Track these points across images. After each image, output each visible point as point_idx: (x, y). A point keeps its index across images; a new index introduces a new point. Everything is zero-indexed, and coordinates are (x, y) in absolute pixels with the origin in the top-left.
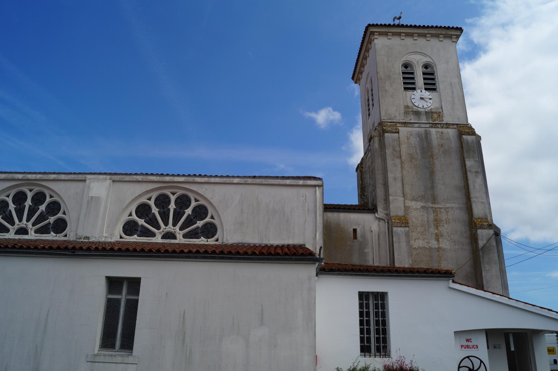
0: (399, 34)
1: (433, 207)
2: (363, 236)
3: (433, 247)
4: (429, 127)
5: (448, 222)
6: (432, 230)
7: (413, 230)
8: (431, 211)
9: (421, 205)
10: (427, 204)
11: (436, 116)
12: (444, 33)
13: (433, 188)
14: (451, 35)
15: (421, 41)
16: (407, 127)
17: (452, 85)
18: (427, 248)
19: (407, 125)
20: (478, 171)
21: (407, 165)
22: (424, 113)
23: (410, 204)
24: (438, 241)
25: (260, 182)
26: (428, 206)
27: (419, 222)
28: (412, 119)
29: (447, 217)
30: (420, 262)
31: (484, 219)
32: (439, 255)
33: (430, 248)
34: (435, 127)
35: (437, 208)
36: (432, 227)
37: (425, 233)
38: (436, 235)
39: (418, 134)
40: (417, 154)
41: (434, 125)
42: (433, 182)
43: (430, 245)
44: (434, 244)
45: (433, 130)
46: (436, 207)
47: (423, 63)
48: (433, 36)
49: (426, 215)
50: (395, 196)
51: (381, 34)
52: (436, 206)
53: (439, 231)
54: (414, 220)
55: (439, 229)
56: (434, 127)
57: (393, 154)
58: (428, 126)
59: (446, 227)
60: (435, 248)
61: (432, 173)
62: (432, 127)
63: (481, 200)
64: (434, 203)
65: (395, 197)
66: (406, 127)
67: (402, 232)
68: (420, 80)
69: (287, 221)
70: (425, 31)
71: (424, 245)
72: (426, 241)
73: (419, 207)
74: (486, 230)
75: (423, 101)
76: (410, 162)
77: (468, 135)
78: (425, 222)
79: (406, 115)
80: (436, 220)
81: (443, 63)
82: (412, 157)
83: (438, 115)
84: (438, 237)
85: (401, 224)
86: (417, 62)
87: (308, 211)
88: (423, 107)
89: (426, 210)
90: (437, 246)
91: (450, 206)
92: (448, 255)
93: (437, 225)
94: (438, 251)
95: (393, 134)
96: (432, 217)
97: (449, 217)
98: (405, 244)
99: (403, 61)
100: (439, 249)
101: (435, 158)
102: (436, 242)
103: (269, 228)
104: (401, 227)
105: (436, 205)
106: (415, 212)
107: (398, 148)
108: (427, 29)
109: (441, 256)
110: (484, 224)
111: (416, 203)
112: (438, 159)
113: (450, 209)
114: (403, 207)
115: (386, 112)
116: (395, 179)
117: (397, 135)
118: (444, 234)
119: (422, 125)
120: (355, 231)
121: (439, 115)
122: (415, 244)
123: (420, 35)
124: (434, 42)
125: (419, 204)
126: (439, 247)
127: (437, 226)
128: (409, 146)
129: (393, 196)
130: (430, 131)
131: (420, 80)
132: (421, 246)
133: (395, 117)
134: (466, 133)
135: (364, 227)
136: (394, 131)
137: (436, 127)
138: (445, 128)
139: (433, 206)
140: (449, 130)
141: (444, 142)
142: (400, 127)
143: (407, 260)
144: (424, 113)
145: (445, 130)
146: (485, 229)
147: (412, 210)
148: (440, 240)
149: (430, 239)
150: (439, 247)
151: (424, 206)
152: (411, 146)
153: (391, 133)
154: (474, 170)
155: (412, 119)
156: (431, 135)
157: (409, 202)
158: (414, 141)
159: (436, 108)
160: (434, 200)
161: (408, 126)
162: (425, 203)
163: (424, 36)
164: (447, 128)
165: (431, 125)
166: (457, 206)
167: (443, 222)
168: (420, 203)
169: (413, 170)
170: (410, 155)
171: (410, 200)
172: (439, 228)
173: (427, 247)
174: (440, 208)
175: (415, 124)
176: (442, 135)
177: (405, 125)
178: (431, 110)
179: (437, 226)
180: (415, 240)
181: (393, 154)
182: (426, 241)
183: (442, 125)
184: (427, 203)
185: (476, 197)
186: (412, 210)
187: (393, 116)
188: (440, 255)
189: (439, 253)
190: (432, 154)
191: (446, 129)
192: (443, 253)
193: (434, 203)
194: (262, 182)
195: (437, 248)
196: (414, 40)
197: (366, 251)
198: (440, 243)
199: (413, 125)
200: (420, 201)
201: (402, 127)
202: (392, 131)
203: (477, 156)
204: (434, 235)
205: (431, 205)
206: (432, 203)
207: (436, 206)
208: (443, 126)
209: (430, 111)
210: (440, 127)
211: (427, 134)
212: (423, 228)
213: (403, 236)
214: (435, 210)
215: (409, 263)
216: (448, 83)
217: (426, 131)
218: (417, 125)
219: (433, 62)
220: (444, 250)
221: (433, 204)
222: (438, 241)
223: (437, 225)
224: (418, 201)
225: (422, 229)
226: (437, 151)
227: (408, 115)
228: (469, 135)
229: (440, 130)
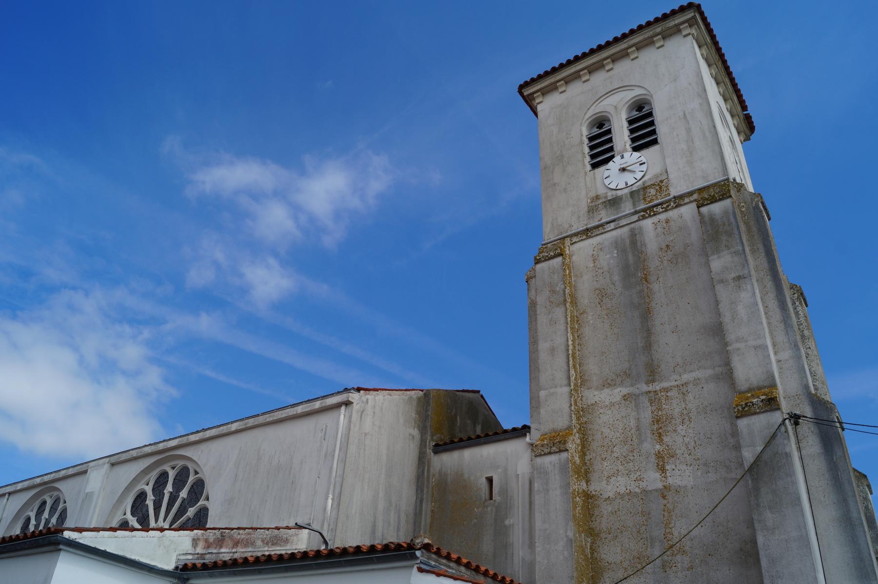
0: (576, 76)
1: (650, 392)
2: (504, 491)
3: (650, 489)
4: (637, 221)
5: (687, 418)
6: (650, 446)
7: (604, 457)
8: (645, 401)
9: (621, 394)
10: (637, 386)
11: (652, 191)
12: (658, 30)
13: (648, 346)
14: (676, 25)
15: (623, 67)
16: (593, 237)
17: (688, 116)
18: (636, 495)
19: (592, 234)
20: (741, 274)
21: (591, 314)
22: (629, 196)
23: (597, 399)
24: (663, 470)
25: (263, 420)
26: (638, 392)
27: (618, 435)
28: (604, 216)
29: (684, 406)
30: (619, 531)
31: (765, 387)
32: (665, 506)
33: (645, 492)
34: (650, 216)
35: (660, 390)
36: (649, 440)
37: (632, 458)
38: (659, 456)
39: (616, 242)
40: (614, 284)
41: (649, 212)
42: (648, 333)
43: (643, 485)
44: (653, 479)
45: (648, 223)
46: (658, 388)
47: (626, 103)
48: (639, 47)
49: (634, 413)
50: (551, 388)
51: (545, 92)
52: (657, 386)
53: (664, 446)
54: (606, 431)
55: (666, 439)
56: (647, 216)
57: (550, 301)
58: (635, 218)
59: (683, 433)
60: (656, 490)
61: (646, 314)
62: (644, 218)
63: (752, 343)
64: (653, 381)
65: (552, 390)
66: (591, 237)
67: (554, 466)
68: (621, 136)
69: (293, 482)
70: (622, 46)
71: (628, 488)
72: (633, 476)
73: (618, 398)
74: (762, 417)
75: (626, 174)
76: (599, 306)
77: (712, 203)
78: (632, 432)
79: (591, 215)
80: (657, 420)
81: (666, 85)
82: (602, 294)
83: (658, 188)
84: (661, 463)
85: (551, 447)
86: (616, 107)
87: (326, 456)
88: (627, 184)
89: (633, 402)
90: (660, 485)
91: (691, 379)
92: (689, 503)
93: (661, 431)
94: (664, 497)
95: (551, 262)
96: (647, 415)
97: (690, 406)
98: (558, 492)
99: (591, 117)
100: (664, 492)
101: (652, 278)
102: (657, 475)
103: (266, 501)
104: (550, 453)
105: (656, 384)
106: (609, 412)
107: (561, 285)
108: (624, 40)
109: (671, 507)
110: (752, 403)
111: (611, 393)
112: (661, 279)
113: (691, 385)
114: (568, 408)
115: (553, 225)
116: (553, 350)
117: (560, 259)
118: (678, 451)
119: (623, 222)
120: (490, 480)
121: (661, 188)
122: (610, 488)
123: (615, 59)
124: (649, 56)
125: (618, 392)
126: (665, 487)
127: (660, 435)
128: (597, 273)
129: (547, 389)
130: (640, 228)
131: (621, 136)
132: (622, 492)
133: (571, 226)
134: (707, 199)
135: (506, 470)
136: (551, 255)
137: (652, 214)
138: (673, 208)
139: (651, 388)
140: (683, 210)
141: (671, 238)
142: (579, 241)
143: (561, 532)
144: (627, 197)
145: (673, 214)
146: (755, 413)
147: (601, 411)
148: (667, 467)
149: (643, 470)
150: (665, 487)
151: (628, 394)
152: (600, 271)
153: (546, 260)
154: (733, 275)
155: (604, 216)
156: (642, 235)
157: (596, 393)
158: (608, 260)
159: (655, 175)
160: (652, 373)
161: (593, 235)
162: (632, 385)
163: (624, 55)
164: (677, 207)
165: (642, 213)
166: (710, 372)
167: (673, 422)
168: (619, 389)
169: (605, 321)
170: (598, 292)
171: (597, 389)
172: (664, 438)
173: (637, 490)
174: (667, 390)
175: (608, 225)
176: (668, 224)
177: (587, 236)
178: (644, 185)
179: (660, 435)
180: (609, 477)
181: (550, 301)
182: (633, 476)
183: (665, 206)
184: (635, 384)
185: (739, 340)
186: (601, 411)
187: (566, 226)
188: (668, 505)
189: (666, 502)
190: (646, 274)
191: (676, 211)
192: (675, 498)
193: (651, 380)
194: (266, 419)
195: (660, 490)
196: (608, 71)
197: (507, 522)
198: (668, 474)
199: (604, 229)
200: (619, 384)
201: (582, 240)
202: (547, 256)
203: (738, 241)
204: (653, 459)
205: (644, 388)
206: (647, 383)
207: (657, 386)
208: (668, 206)
209: (643, 186)
210: (661, 210)
211: (636, 235)
212: (627, 447)
213: (555, 474)
214: (654, 398)
215: (567, 536)
216: (679, 116)
217: (632, 231)
218: (612, 225)
219: (650, 94)
220: (678, 490)
221: (650, 385)
222: (663, 470)
223: (661, 431)
224: (615, 387)
225: (624, 449)
226: (658, 263)
227: (595, 214)
228: (716, 201)
229: (663, 217)
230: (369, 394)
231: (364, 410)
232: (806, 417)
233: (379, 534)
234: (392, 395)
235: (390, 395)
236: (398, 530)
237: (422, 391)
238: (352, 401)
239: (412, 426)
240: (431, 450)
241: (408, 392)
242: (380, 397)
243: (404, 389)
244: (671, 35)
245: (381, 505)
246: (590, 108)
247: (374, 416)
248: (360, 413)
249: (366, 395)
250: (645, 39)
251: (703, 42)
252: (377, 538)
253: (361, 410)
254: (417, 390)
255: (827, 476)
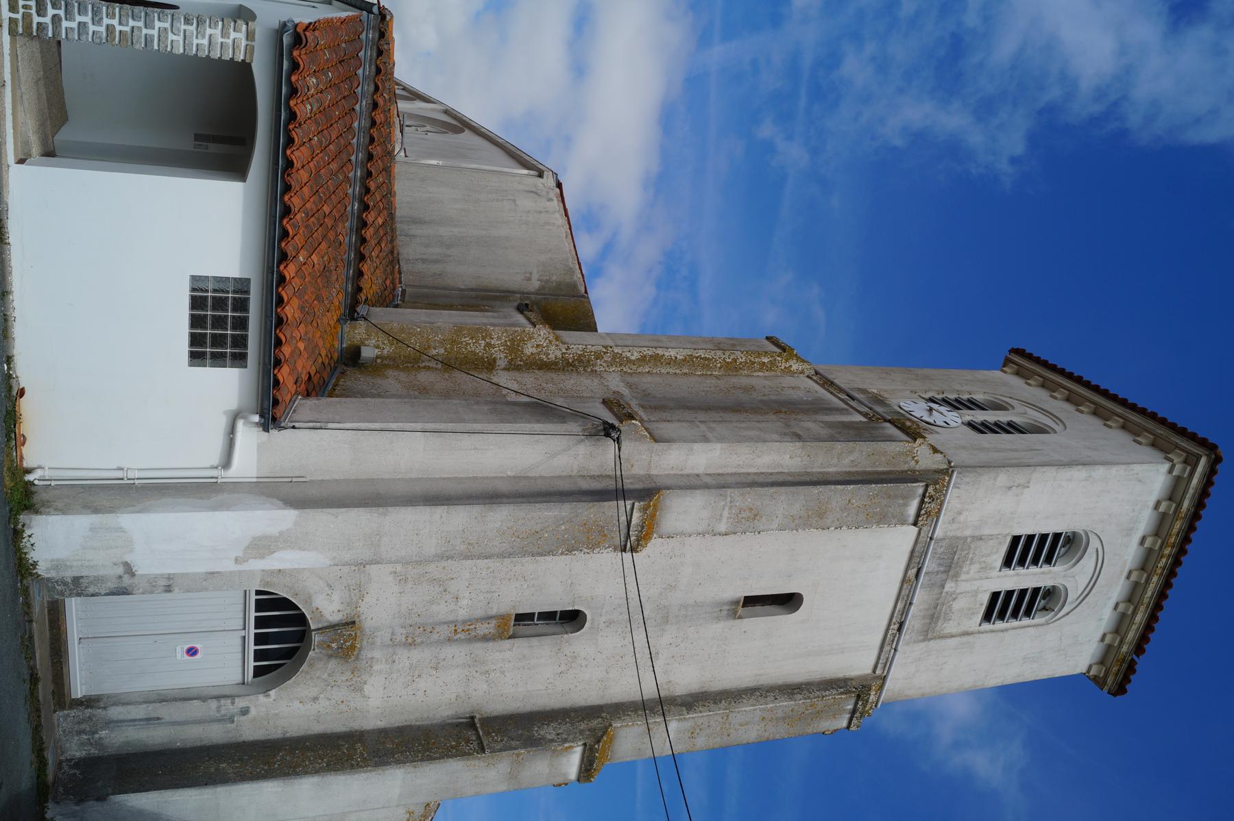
218: (844, 397)
230: (558, 201)
231: (539, 195)
232: (619, 450)
233: (415, 230)
234: (568, 239)
235: (566, 237)
236: (424, 261)
237: (586, 292)
238: (545, 176)
239: (541, 276)
240: (519, 301)
241: (577, 266)
242: (561, 220)
243: (584, 273)
244: (1162, 450)
245: (444, 231)
246: (1013, 399)
247: (536, 212)
248: (533, 189)
249: (557, 197)
250: (1138, 425)
251: (1178, 498)
252: (410, 227)
253: (538, 192)
254: (584, 281)
255: (552, 489)
